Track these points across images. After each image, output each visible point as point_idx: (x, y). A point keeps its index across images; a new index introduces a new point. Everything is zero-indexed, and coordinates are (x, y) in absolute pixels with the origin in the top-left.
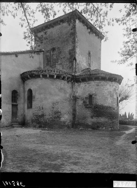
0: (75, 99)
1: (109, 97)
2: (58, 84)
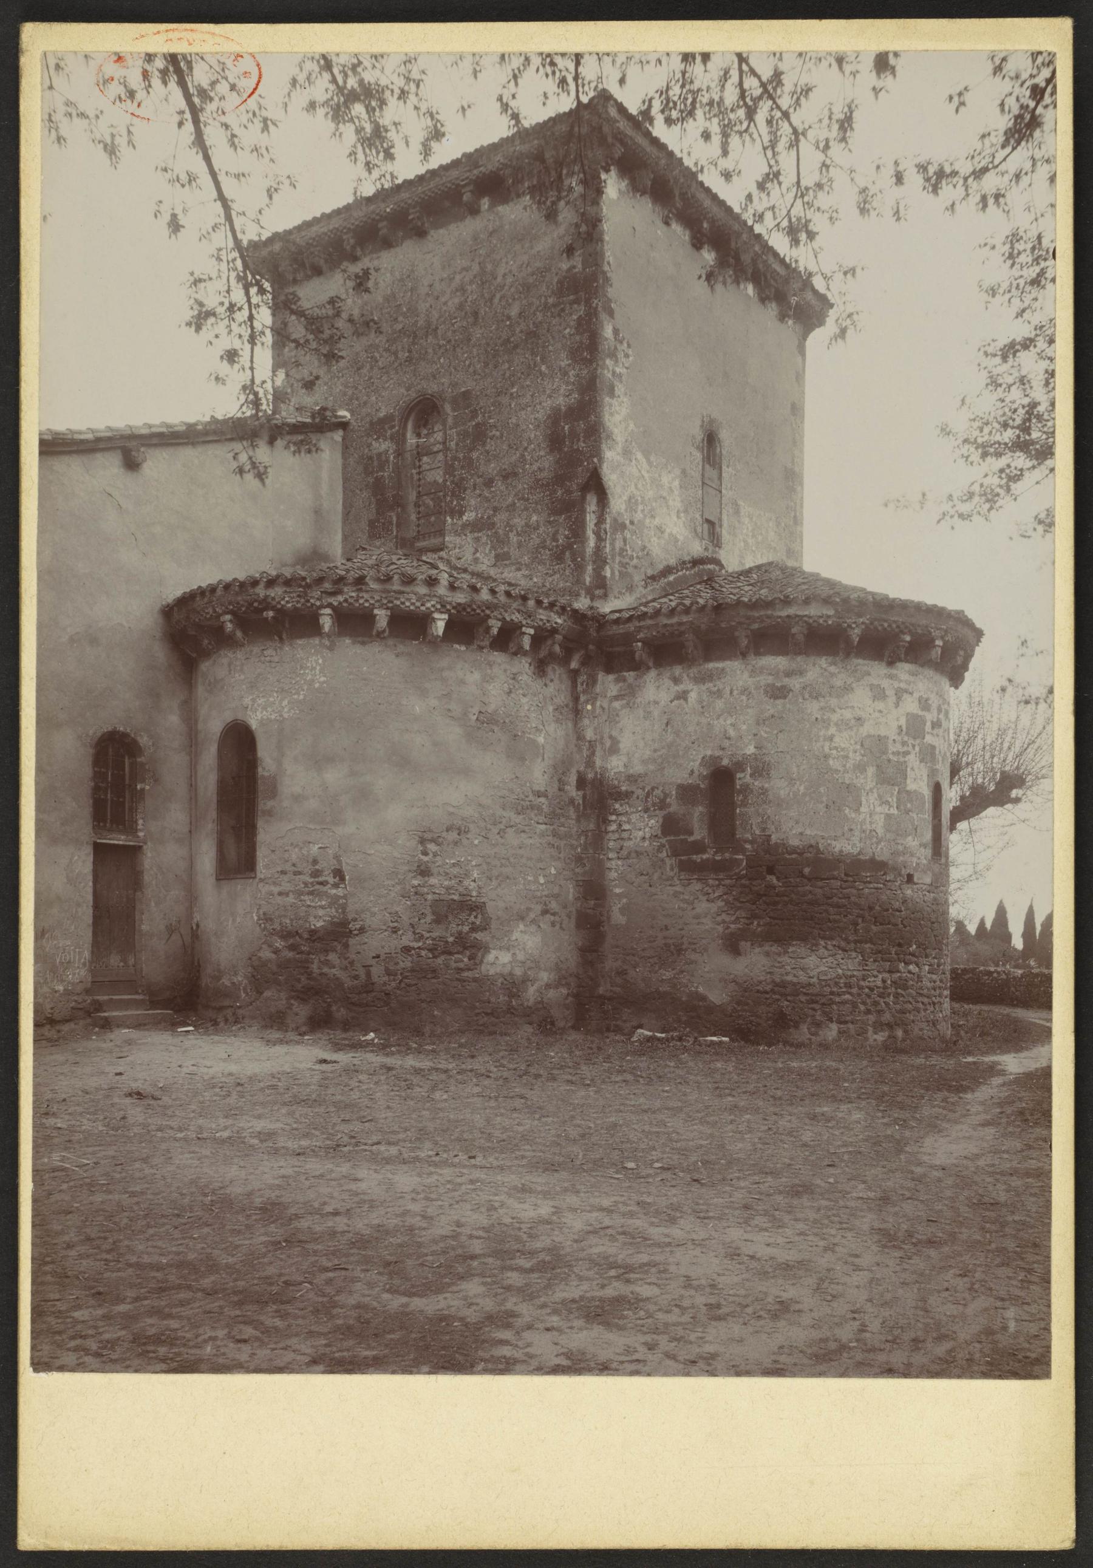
1: (870, 784)
2: (462, 682)
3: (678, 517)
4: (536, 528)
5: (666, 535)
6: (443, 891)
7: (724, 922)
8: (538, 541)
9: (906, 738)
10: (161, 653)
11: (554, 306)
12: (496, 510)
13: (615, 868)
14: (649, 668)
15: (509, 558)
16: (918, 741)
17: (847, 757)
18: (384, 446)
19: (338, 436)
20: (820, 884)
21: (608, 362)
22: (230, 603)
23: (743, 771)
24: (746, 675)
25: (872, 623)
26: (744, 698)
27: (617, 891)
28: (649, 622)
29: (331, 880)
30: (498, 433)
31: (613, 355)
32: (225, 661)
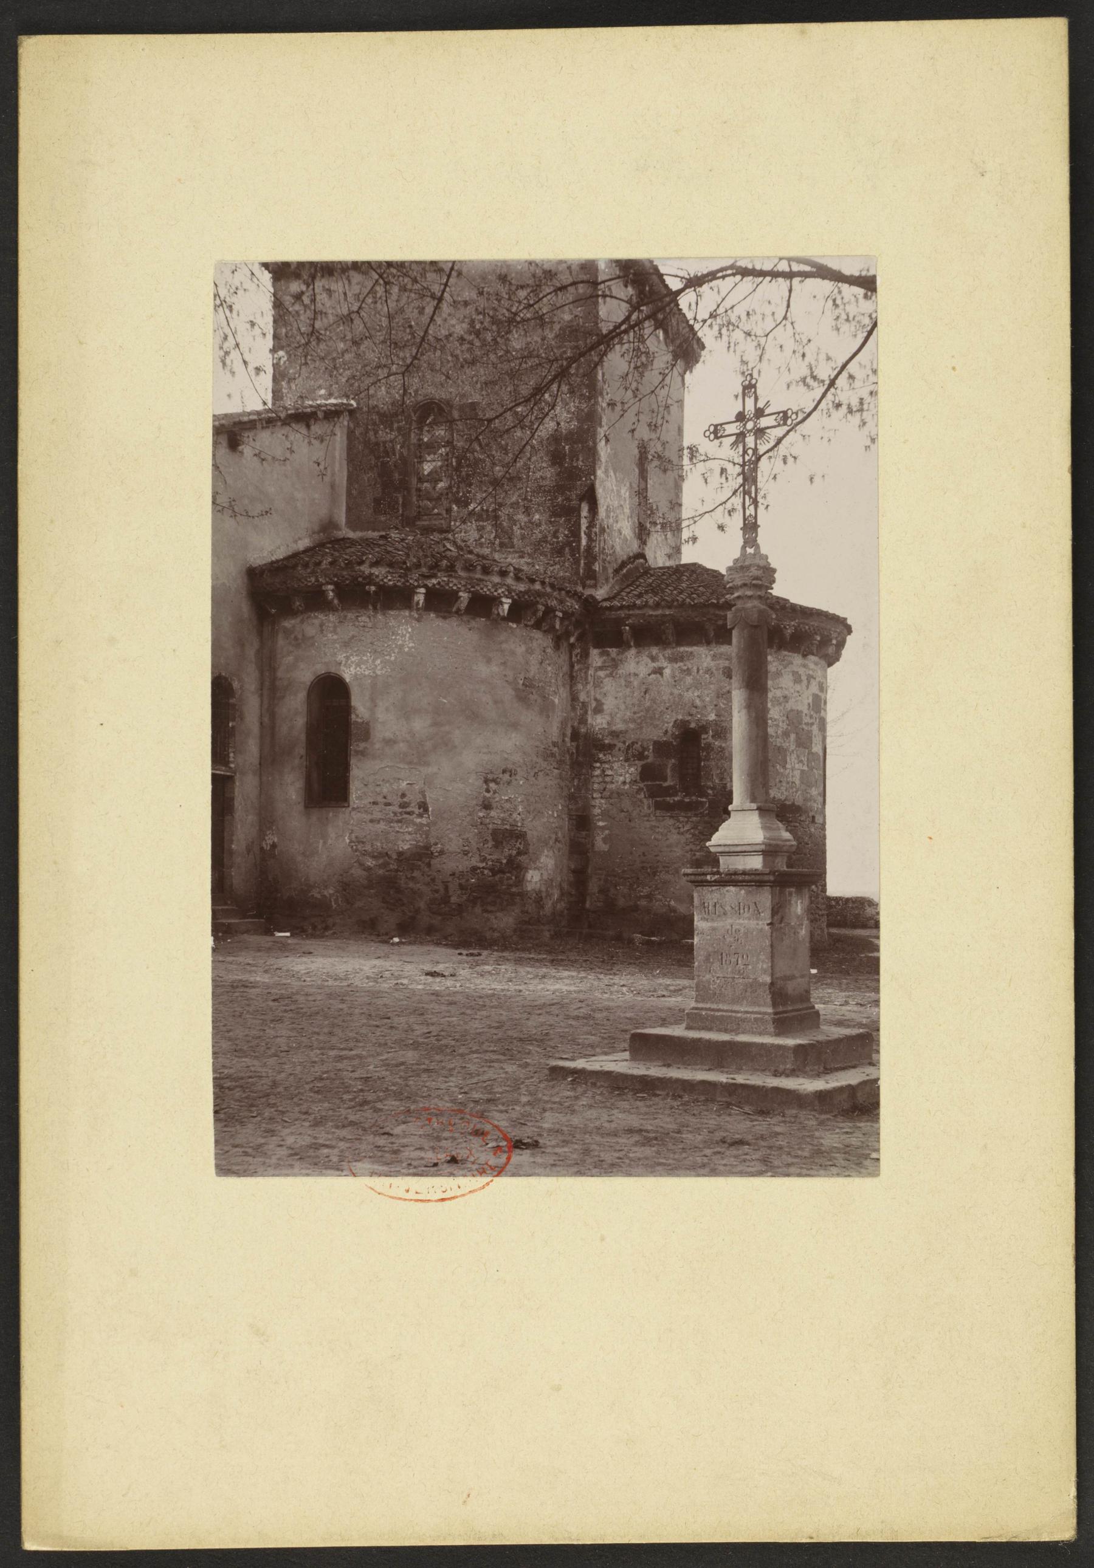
0: (583, 751)
1: (793, 747)
2: (513, 653)
4: (539, 525)
7: (691, 850)
8: (540, 536)
10: (246, 609)
12: (501, 505)
13: (599, 805)
14: (630, 647)
17: (777, 726)
22: (335, 576)
23: (707, 733)
24: (709, 659)
27: (601, 824)
28: (637, 612)
29: (417, 811)
32: (317, 622)
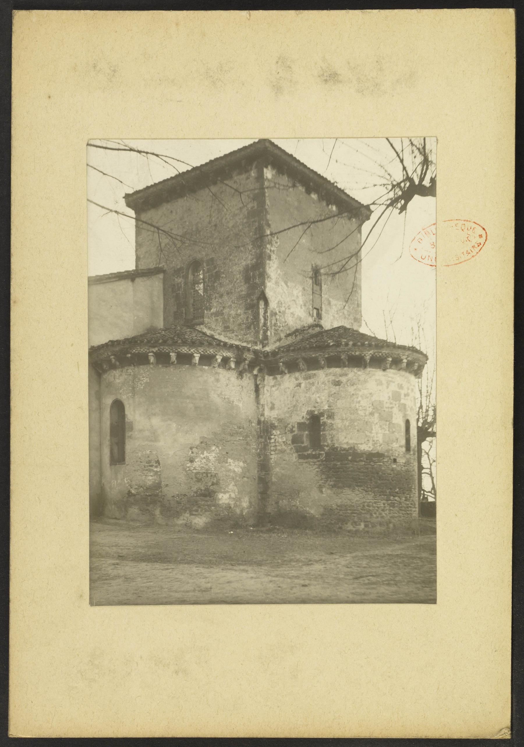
1: (376, 421)
3: (301, 308)
4: (240, 315)
5: (296, 316)
6: (200, 469)
9: (392, 401)
11: (246, 223)
12: (224, 307)
14: (286, 373)
15: (229, 328)
16: (397, 402)
17: (365, 410)
18: (180, 280)
19: (161, 276)
20: (355, 463)
21: (268, 246)
23: (323, 416)
25: (374, 354)
26: (323, 386)
29: (155, 464)
30: (224, 276)
31: (270, 243)
32: (113, 374)
